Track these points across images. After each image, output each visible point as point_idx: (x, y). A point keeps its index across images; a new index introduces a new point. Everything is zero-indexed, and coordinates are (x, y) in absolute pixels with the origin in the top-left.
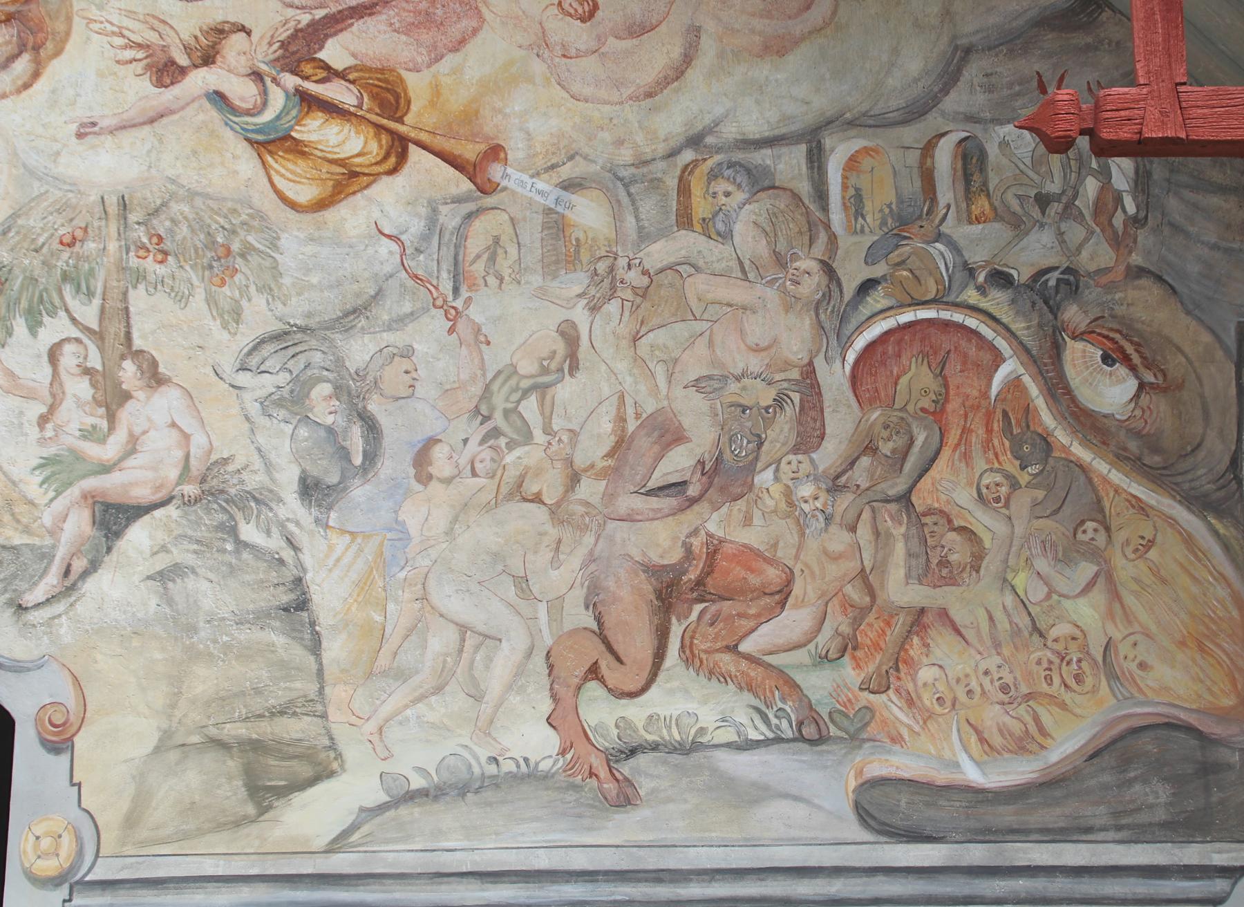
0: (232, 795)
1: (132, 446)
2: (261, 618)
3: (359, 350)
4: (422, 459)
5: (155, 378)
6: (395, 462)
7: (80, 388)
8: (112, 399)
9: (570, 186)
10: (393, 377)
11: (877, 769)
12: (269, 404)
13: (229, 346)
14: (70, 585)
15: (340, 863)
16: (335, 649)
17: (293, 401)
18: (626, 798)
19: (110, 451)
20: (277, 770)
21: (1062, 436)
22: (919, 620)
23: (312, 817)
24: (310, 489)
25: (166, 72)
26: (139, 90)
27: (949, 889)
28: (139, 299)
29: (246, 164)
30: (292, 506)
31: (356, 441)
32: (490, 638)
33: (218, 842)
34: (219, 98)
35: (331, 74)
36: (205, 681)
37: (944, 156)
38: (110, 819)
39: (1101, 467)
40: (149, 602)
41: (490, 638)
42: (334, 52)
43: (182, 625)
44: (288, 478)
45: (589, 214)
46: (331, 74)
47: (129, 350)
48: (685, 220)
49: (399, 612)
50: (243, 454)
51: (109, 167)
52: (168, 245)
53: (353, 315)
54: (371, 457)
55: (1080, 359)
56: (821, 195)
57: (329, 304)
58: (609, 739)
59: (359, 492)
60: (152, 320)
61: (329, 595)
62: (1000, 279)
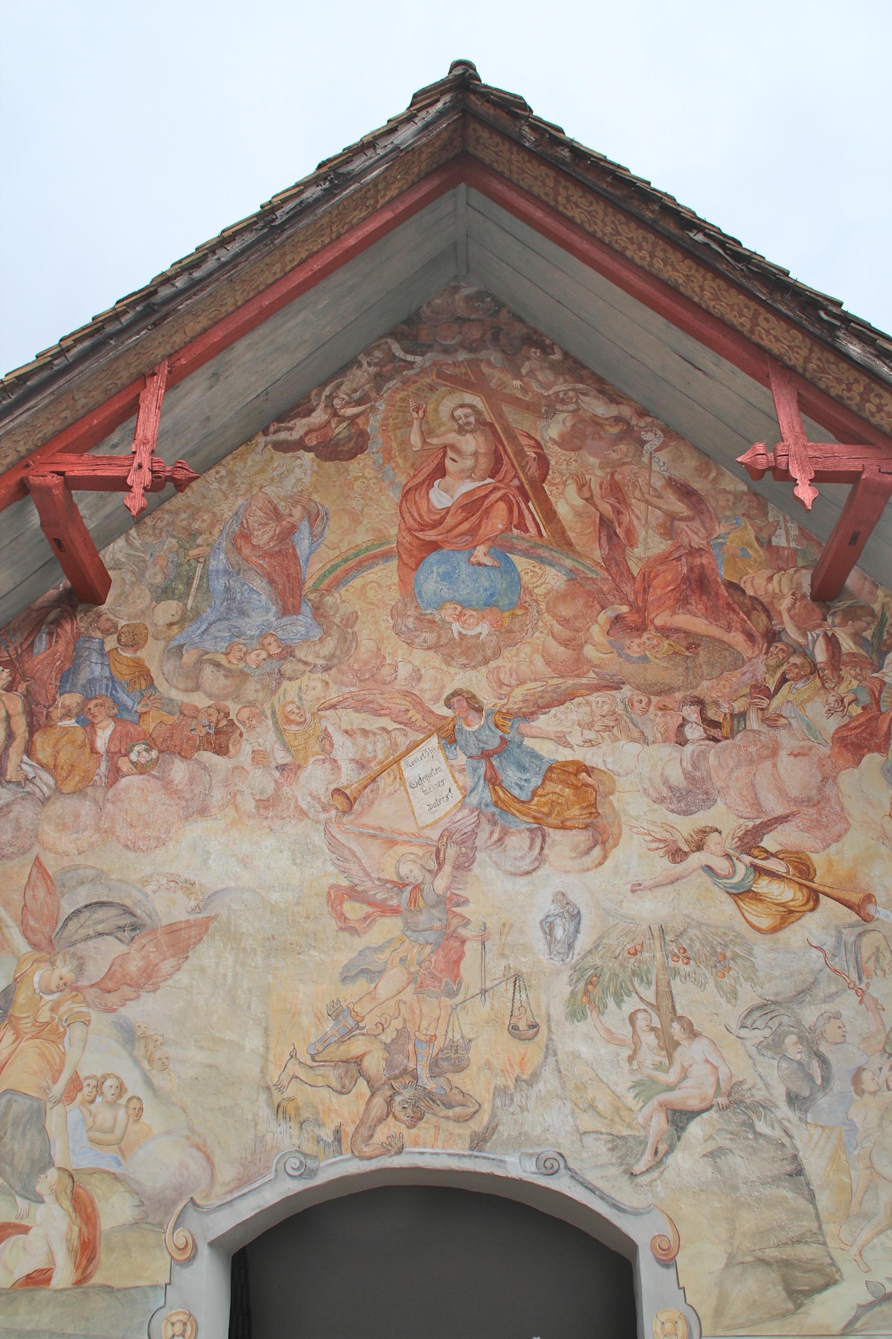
0: (777, 1295)
1: (684, 1074)
2: (776, 1180)
3: (809, 1015)
4: (856, 1079)
5: (693, 1033)
6: (841, 1083)
7: (649, 1039)
8: (669, 1046)
13: (732, 1013)
14: (658, 1162)
16: (824, 1200)
17: (775, 1045)
19: (672, 1077)
24: (793, 1099)
25: (677, 855)
26: (663, 865)
28: (677, 986)
29: (728, 906)
30: (784, 1110)
31: (815, 1069)
34: (708, 869)
35: (769, 855)
36: (748, 1221)
40: (707, 1172)
42: (769, 842)
44: (779, 1093)
46: (769, 855)
47: (675, 1016)
51: (650, 909)
53: (803, 993)
59: (823, 1101)
60: (687, 998)
61: (815, 1166)
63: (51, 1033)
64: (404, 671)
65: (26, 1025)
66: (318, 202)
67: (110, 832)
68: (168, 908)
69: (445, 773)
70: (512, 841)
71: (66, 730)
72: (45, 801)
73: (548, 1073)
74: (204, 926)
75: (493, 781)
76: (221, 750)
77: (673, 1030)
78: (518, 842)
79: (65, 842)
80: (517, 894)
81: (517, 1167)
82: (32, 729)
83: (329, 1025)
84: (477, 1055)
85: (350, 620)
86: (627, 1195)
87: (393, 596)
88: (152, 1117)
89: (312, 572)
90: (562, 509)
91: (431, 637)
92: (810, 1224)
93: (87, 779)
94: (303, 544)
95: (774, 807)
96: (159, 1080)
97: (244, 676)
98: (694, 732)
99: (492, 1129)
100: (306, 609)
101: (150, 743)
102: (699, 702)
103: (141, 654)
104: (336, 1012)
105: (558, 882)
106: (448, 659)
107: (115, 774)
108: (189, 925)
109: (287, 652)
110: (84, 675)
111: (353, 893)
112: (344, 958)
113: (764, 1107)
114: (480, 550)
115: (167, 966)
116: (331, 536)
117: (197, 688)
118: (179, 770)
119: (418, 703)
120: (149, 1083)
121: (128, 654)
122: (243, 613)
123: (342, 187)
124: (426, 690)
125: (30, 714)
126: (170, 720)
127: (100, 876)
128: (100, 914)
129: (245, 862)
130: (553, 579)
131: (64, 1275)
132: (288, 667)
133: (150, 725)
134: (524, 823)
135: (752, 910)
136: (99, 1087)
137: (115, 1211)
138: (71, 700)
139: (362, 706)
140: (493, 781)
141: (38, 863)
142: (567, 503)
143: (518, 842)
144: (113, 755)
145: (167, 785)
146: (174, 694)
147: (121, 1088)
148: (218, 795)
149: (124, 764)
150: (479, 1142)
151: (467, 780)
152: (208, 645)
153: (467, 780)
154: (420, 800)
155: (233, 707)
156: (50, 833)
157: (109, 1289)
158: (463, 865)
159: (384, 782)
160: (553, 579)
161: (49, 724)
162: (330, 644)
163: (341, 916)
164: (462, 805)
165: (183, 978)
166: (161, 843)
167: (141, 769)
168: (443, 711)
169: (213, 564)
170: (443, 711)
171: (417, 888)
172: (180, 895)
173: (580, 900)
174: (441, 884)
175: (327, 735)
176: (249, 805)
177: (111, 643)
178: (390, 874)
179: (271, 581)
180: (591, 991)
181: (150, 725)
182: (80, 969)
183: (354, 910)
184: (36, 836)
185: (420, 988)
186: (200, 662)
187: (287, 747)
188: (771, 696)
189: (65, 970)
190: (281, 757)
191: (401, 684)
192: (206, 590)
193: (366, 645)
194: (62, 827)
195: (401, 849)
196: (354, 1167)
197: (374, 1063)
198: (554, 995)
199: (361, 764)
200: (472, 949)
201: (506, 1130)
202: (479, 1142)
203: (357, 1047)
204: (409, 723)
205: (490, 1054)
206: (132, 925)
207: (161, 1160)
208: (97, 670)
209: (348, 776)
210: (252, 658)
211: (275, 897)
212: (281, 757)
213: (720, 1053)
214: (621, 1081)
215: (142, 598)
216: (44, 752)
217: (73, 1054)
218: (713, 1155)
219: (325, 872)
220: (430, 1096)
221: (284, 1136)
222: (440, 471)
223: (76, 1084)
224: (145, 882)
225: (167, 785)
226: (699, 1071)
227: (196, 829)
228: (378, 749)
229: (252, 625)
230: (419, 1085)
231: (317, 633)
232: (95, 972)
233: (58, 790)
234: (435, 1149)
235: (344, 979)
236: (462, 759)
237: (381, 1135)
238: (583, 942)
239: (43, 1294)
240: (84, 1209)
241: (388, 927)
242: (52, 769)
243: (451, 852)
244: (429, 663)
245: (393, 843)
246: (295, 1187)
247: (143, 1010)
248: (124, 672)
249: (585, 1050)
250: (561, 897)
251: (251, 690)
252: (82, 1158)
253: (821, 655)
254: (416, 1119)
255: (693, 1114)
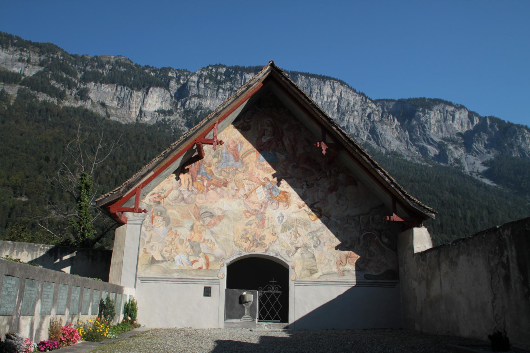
0: (309, 274)
1: (298, 242)
2: (310, 258)
3: (318, 234)
4: (324, 244)
5: (300, 236)
6: (322, 244)
7: (293, 236)
8: (296, 237)
9: (337, 219)
10: (321, 236)
11: (366, 273)
12: (310, 238)
13: (307, 233)
14: (293, 254)
15: (319, 280)
16: (317, 261)
17: (313, 238)
18: (344, 275)
19: (296, 242)
20: (313, 272)
21: (381, 244)
22: (369, 260)
23: (316, 276)
24: (314, 246)
25: (300, 207)
26: (298, 209)
27: (171, 168)
28: (298, 228)
29: (307, 216)
30: (313, 248)
31: (318, 242)
32: (331, 261)
33: (308, 278)
34: (305, 210)
35: (315, 208)
36: (306, 263)
37: (371, 218)
38: (298, 275)
39: (385, 247)
40: (300, 256)
41: (331, 261)
42: (315, 206)
43: (303, 258)
44: (312, 245)
45: (339, 222)
46: (315, 208)
47: (297, 233)
48: (347, 223)
49: (323, 258)
50: (308, 243)
51: (294, 216)
52: (271, 187)
53: (317, 231)
54: (320, 244)
55: (383, 237)
56: (359, 221)
57: (315, 229)
58: (342, 270)
59: (319, 247)
60: (300, 230)
61: (316, 256)
62: (376, 229)
63: (200, 232)
64: (257, 173)
65: (196, 231)
66: (245, 91)
67: (208, 200)
68: (218, 213)
69: (263, 192)
70: (274, 204)
71: (199, 182)
72: (196, 194)
73: (277, 241)
74: (224, 216)
75: (271, 194)
76: (226, 186)
77: (297, 235)
78: (275, 204)
79: (200, 201)
80: (273, 213)
81: (272, 254)
82: (193, 181)
83: (244, 232)
84: (266, 238)
85: (248, 164)
86: (288, 259)
87: (255, 159)
88: (216, 245)
89: (241, 154)
90: (285, 143)
91: (261, 167)
92: (315, 264)
93: (203, 191)
94: (239, 149)
95: (317, 200)
96: (218, 240)
97: (229, 173)
98: (305, 187)
99: (268, 249)
100: (240, 161)
101: (214, 185)
102: (306, 181)
103: (211, 168)
104: (245, 230)
105: (280, 211)
106: (264, 172)
107: (208, 190)
108: (221, 216)
109: (237, 169)
110: (201, 172)
111: (248, 212)
112: (246, 222)
113: (310, 247)
114: (270, 151)
115: (218, 222)
116: (244, 147)
117: (221, 175)
118: (219, 190)
119: (259, 179)
120: (216, 240)
121: (209, 168)
122: (229, 161)
123: (249, 88)
124: (260, 177)
125: (192, 179)
126: (217, 181)
127: (206, 207)
128: (207, 214)
129: (230, 206)
130: (283, 157)
131: (204, 267)
132: (237, 172)
133: (213, 181)
134: (276, 201)
135: (311, 217)
136: (208, 241)
137: (211, 259)
138: (199, 176)
139: (250, 179)
140: (271, 194)
141: (196, 205)
142: (286, 142)
143: (275, 204)
144: (207, 187)
145: (217, 192)
146: (217, 176)
147: (211, 241)
148: (225, 194)
149: (209, 188)
150: (266, 250)
151: (267, 193)
152: (223, 167)
153: (267, 193)
154: (259, 197)
155: (227, 179)
156: (197, 200)
157: (211, 270)
158: (265, 208)
159: (253, 193)
160: (283, 157)
161: (196, 181)
162: (244, 168)
163: (246, 215)
164: (266, 197)
165: (220, 224)
166: (216, 202)
167: (212, 189)
168: (263, 181)
169: (223, 151)
170: (263, 181)
171: (258, 211)
172: (220, 211)
173: (284, 214)
174: (262, 211)
175: (243, 185)
176: (231, 196)
177: (206, 166)
178: (254, 209)
179: (234, 155)
180: (285, 228)
181: (213, 181)
182: (204, 222)
183: (248, 214)
184: (195, 200)
185: (258, 227)
186: (221, 170)
187: (237, 186)
188: (318, 181)
189: (201, 223)
190: (236, 188)
191: (256, 176)
192: (222, 157)
193: (250, 168)
194: (199, 199)
195: (255, 205)
196: (248, 254)
197: (251, 238)
198: (279, 229)
199: (249, 190)
200: (266, 221)
201: (271, 249)
202: (266, 250)
203: (248, 236)
204: (257, 183)
205: (269, 238)
206: (212, 215)
207: (218, 251)
208: (204, 171)
209: (247, 192)
210: (230, 170)
211: (235, 212)
212: (236, 188)
213: (304, 238)
214: (288, 242)
215: (211, 158)
216: (195, 185)
217: (204, 236)
218: (302, 254)
219: (243, 208)
220: (259, 243)
221: (237, 249)
222: (264, 135)
223: (204, 240)
224: (214, 208)
225: (217, 192)
226: (301, 241)
227: (222, 200)
228: (252, 187)
229: (230, 164)
230: (258, 241)
231: (242, 166)
232: (207, 223)
233: (198, 192)
234: (259, 251)
235: (246, 225)
236: (266, 190)
237: (252, 249)
238: (284, 221)
239: (201, 270)
240: (207, 258)
241: (253, 217)
242: (197, 189)
243: (264, 205)
244: (261, 172)
245: (254, 203)
246: (239, 256)
247: (215, 229)
248: (208, 172)
249: (283, 237)
250: (281, 213)
251: (231, 175)
252: (206, 252)
253: (328, 174)
254: (257, 247)
255: (299, 248)
